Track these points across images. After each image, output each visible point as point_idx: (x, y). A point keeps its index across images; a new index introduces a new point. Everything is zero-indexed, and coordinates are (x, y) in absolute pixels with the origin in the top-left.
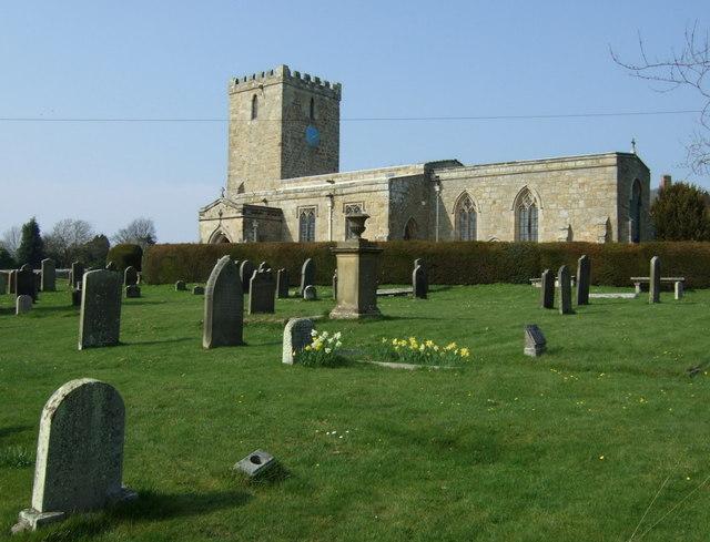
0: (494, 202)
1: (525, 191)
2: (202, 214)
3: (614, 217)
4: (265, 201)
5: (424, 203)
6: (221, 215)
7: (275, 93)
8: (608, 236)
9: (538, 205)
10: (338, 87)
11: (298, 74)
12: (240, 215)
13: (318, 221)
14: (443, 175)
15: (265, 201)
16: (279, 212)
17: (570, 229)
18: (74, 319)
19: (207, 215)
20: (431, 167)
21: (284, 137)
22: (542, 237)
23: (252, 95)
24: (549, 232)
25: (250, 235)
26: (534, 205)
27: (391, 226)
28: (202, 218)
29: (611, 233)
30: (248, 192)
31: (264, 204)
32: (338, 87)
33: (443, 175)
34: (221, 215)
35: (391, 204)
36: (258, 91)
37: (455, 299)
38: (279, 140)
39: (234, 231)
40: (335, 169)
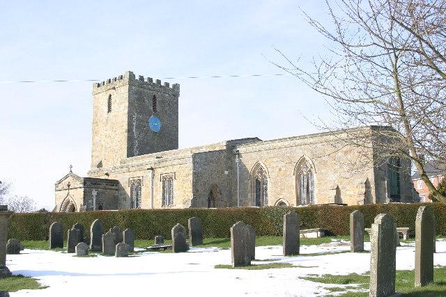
0: (280, 170)
1: (303, 160)
2: (57, 185)
3: (371, 177)
4: (107, 174)
5: (226, 172)
6: (69, 186)
7: (122, 96)
8: (367, 194)
9: (313, 170)
10: (176, 87)
11: (142, 78)
12: (82, 185)
13: (143, 189)
14: (241, 149)
15: (107, 174)
16: (116, 183)
17: (338, 188)
18: (255, 203)
19: (60, 187)
20: (232, 145)
21: (130, 124)
22: (318, 200)
23: (108, 94)
24: (322, 196)
25: (90, 201)
26: (310, 171)
27: (195, 191)
28: (57, 189)
29: (370, 192)
30: (199, 130)
31: (106, 177)
32: (176, 87)
33: (241, 149)
34: (69, 186)
35: (194, 173)
36: (112, 92)
37: (439, 223)
38: (126, 127)
39: (77, 197)
40: (176, 147)
